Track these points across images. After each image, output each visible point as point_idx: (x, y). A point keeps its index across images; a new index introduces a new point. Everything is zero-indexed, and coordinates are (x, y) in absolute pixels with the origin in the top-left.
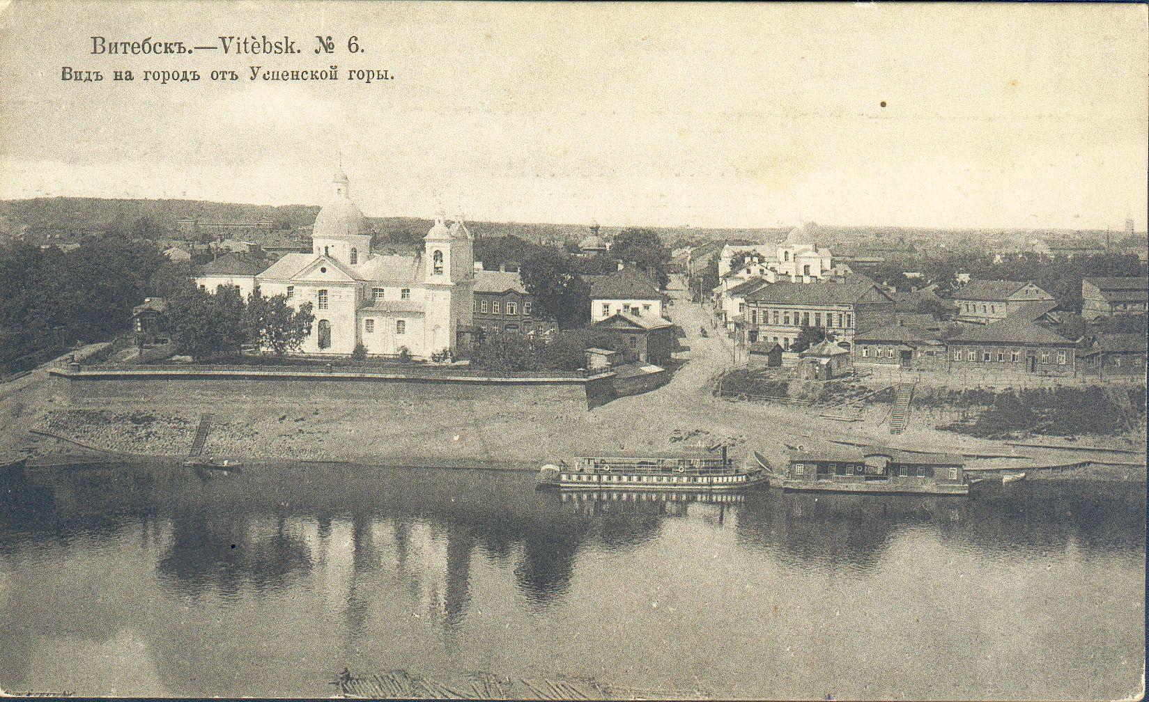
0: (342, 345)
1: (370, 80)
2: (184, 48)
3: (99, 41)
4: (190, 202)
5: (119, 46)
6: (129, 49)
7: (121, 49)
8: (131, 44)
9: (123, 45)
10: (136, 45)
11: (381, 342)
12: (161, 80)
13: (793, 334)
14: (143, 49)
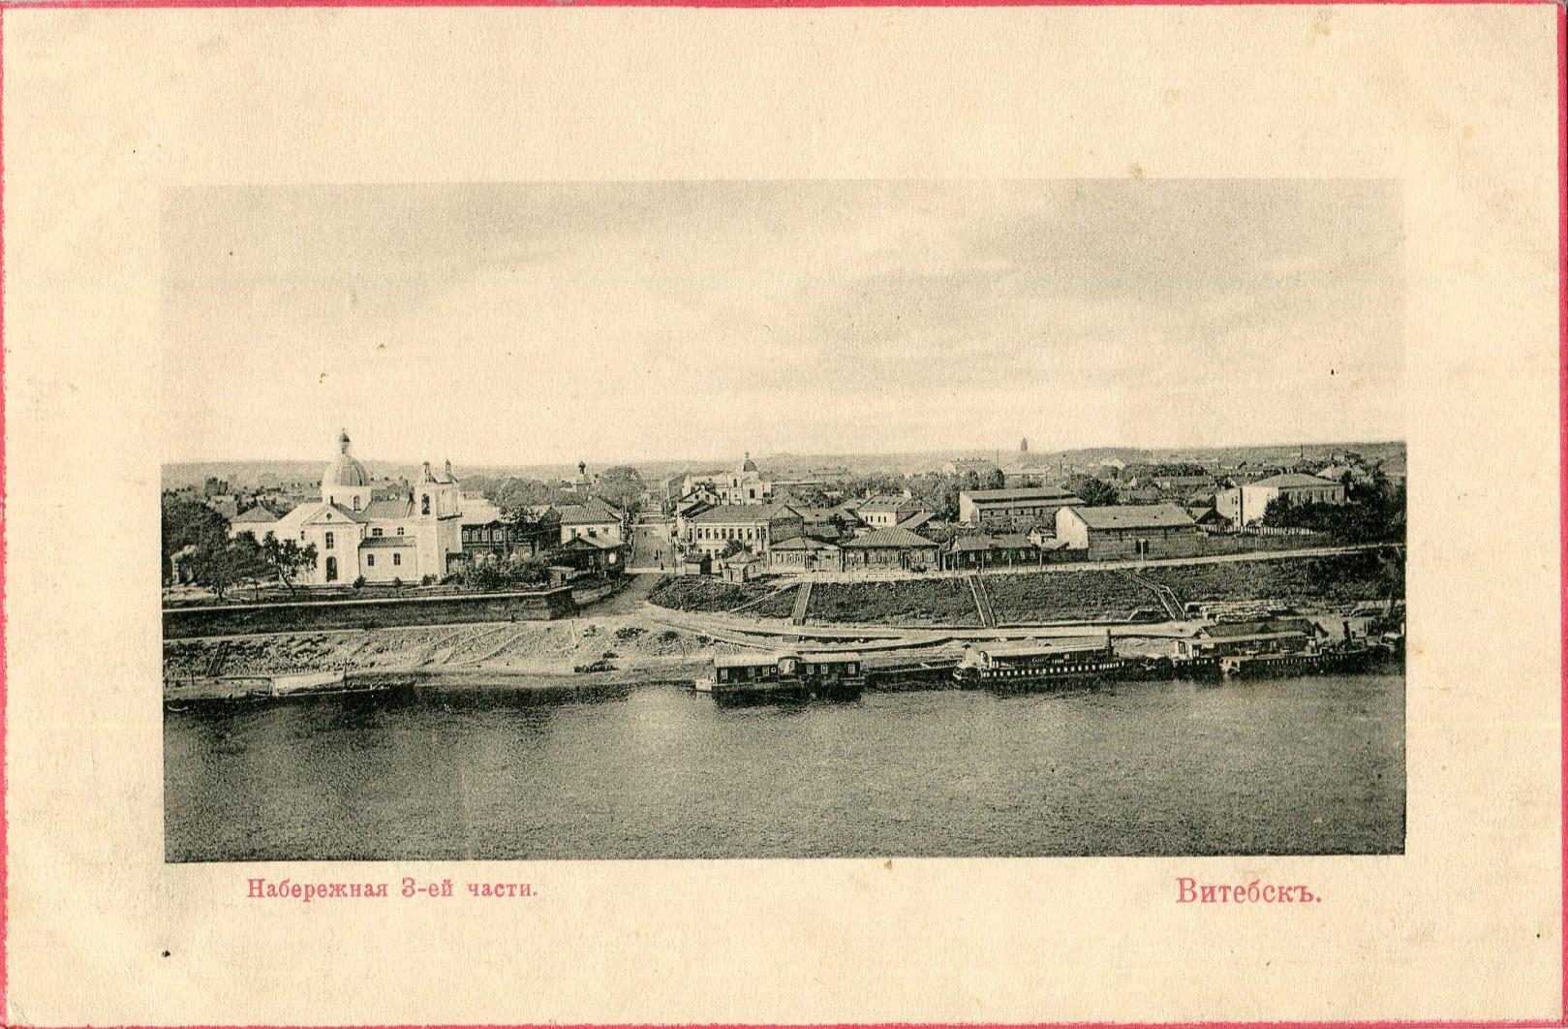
0: (347, 576)
1: (310, 899)
2: (1310, 894)
3: (1188, 884)
4: (816, 7)
5: (1216, 890)
6: (1230, 895)
7: (1219, 896)
8: (1233, 889)
9: (1222, 890)
10: (1239, 890)
11: (383, 572)
12: (303, 897)
13: (722, 545)
14: (1249, 896)
